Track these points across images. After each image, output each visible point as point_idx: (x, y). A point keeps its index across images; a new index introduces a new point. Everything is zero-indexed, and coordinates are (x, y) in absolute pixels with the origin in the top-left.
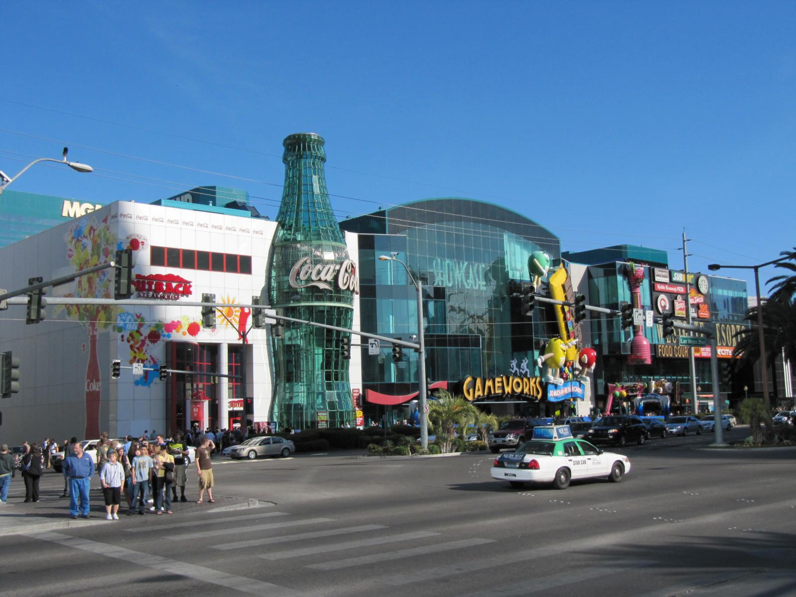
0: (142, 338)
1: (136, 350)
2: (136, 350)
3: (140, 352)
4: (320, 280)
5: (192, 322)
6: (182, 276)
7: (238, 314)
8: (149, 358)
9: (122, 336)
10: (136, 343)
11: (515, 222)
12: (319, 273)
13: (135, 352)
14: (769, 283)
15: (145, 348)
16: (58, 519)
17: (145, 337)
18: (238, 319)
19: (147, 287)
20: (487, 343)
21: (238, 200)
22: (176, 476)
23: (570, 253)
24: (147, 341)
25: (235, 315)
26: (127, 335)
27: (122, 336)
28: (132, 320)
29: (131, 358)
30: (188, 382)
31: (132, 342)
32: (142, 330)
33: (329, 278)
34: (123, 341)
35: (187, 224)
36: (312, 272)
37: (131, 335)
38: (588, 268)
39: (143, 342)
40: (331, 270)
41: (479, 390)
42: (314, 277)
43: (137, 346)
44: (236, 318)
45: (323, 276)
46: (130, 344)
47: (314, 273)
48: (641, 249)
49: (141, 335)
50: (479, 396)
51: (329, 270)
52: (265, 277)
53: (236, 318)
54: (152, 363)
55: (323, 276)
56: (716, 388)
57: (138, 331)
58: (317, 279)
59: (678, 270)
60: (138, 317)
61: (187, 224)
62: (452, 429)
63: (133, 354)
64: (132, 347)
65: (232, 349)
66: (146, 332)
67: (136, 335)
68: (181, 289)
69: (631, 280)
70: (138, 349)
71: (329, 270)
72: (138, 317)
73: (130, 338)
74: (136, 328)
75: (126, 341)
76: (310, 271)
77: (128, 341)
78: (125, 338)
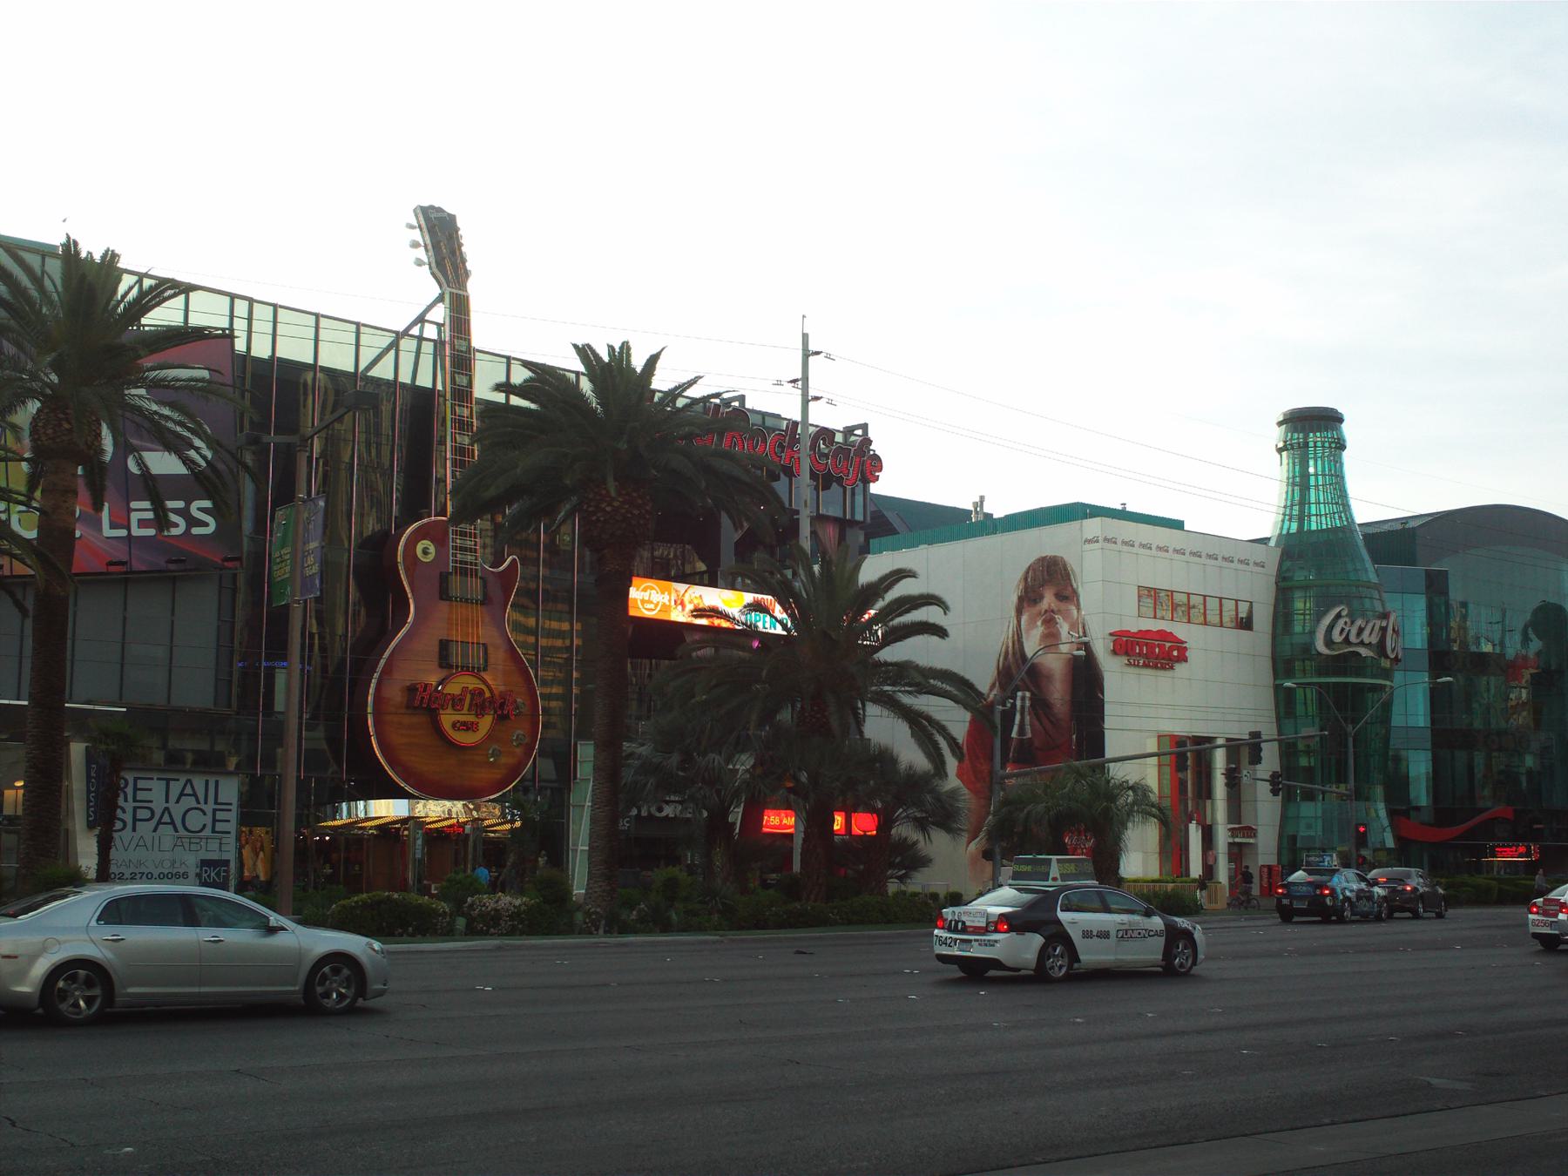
4: (1362, 643)
11: (264, 693)
12: (1361, 630)
16: (1122, 757)
20: (932, 734)
21: (1280, 519)
23: (995, 517)
33: (1374, 640)
36: (1350, 630)
38: (87, 747)
40: (1377, 628)
42: (1353, 638)
45: (1365, 637)
47: (1354, 631)
48: (60, 960)
51: (1374, 626)
52: (956, 671)
55: (1365, 637)
56: (1530, 923)
58: (1358, 641)
59: (663, 353)
69: (1141, 604)
71: (1374, 626)
76: (1347, 629)
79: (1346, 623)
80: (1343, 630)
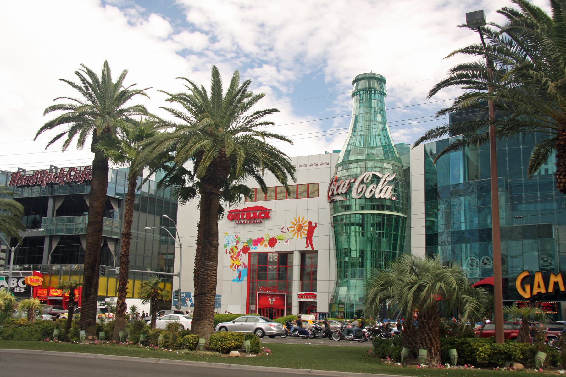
0: (239, 250)
1: (234, 259)
2: (234, 259)
3: (236, 260)
4: (338, 194)
5: (272, 237)
6: (264, 206)
7: (307, 228)
8: (242, 264)
9: (227, 251)
10: (234, 255)
13: (234, 260)
14: (169, 113)
15: (240, 257)
17: (240, 250)
18: (306, 232)
19: (241, 217)
22: (140, 347)
24: (241, 253)
25: (304, 229)
26: (229, 250)
27: (227, 251)
28: (233, 240)
29: (231, 264)
30: (131, 279)
31: (232, 254)
32: (238, 246)
34: (226, 253)
35: (312, 165)
37: (232, 249)
39: (239, 253)
41: (539, 286)
43: (235, 256)
44: (304, 231)
46: (230, 255)
49: (238, 249)
50: (539, 293)
53: (304, 231)
54: (244, 267)
57: (236, 247)
60: (236, 237)
61: (312, 165)
62: (517, 327)
63: (233, 262)
64: (231, 257)
65: (303, 254)
66: (241, 246)
67: (235, 249)
68: (263, 215)
70: (235, 258)
72: (236, 237)
73: (231, 251)
74: (235, 245)
75: (228, 253)
77: (230, 253)
78: (228, 252)
79: (373, 187)
80: (371, 191)
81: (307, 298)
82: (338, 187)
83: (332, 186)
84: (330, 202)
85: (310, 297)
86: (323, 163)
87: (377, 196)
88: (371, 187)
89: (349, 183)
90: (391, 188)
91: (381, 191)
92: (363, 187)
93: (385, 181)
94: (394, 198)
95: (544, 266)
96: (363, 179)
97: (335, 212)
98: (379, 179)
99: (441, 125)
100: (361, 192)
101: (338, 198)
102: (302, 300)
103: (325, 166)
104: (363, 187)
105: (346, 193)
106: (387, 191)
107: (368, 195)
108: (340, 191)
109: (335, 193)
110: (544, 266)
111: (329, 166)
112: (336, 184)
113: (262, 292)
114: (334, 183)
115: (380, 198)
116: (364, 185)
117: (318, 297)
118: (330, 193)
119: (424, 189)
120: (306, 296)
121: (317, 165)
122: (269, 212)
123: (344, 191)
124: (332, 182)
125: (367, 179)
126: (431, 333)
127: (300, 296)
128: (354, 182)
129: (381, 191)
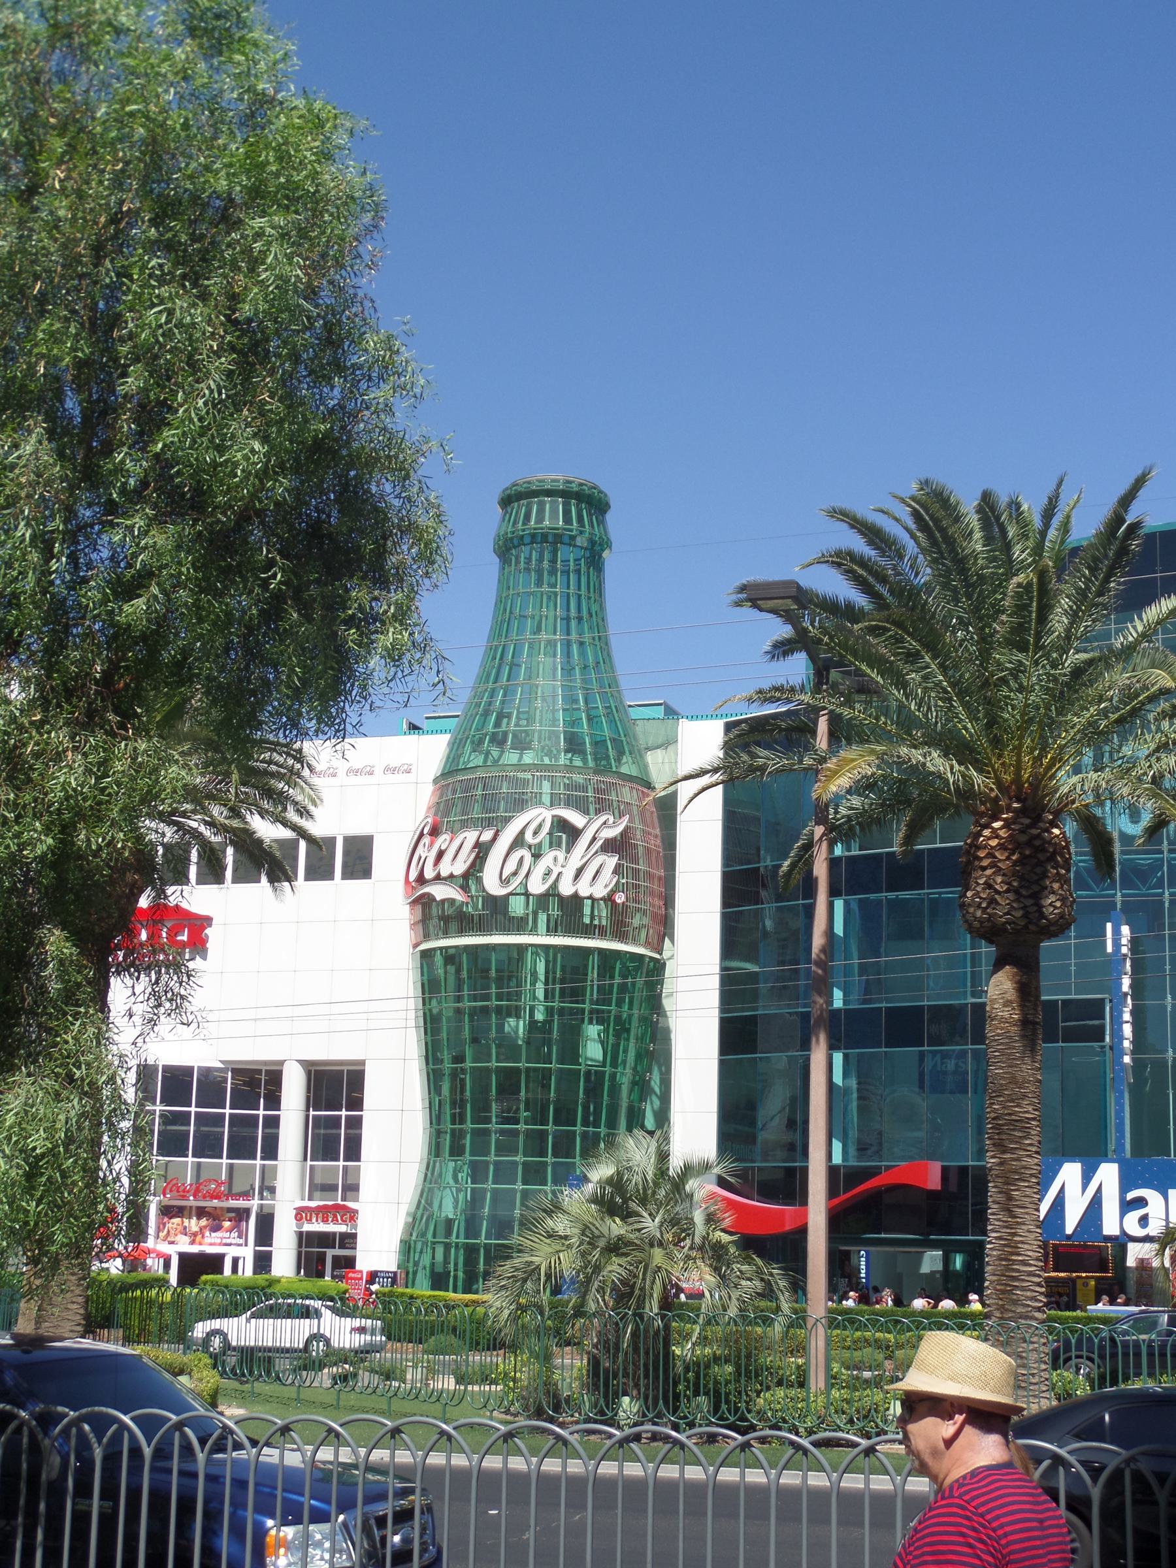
4: (438, 877)
68: (184, 938)
79: (555, 859)
80: (548, 873)
81: (325, 1220)
82: (440, 855)
83: (420, 850)
84: (414, 902)
85: (335, 1216)
86: (393, 765)
87: (566, 889)
88: (546, 861)
89: (477, 845)
90: (612, 861)
91: (579, 872)
92: (521, 861)
93: (594, 839)
94: (620, 898)
95: (762, 1311)
96: (522, 833)
97: (427, 937)
98: (574, 834)
99: (781, 681)
100: (515, 874)
101: (440, 892)
102: (307, 1227)
103: (400, 777)
104: (521, 861)
105: (466, 876)
106: (597, 872)
107: (537, 886)
108: (445, 869)
109: (429, 874)
110: (762, 1311)
111: (411, 777)
112: (432, 844)
113: (168, 1199)
114: (426, 840)
115: (575, 896)
116: (524, 852)
117: (361, 1220)
118: (413, 875)
119: (716, 969)
120: (324, 1213)
121: (371, 773)
122: (203, 928)
123: (459, 868)
124: (421, 835)
125: (535, 833)
126: (886, 1433)
127: (301, 1214)
128: (494, 839)
129: (579, 872)
